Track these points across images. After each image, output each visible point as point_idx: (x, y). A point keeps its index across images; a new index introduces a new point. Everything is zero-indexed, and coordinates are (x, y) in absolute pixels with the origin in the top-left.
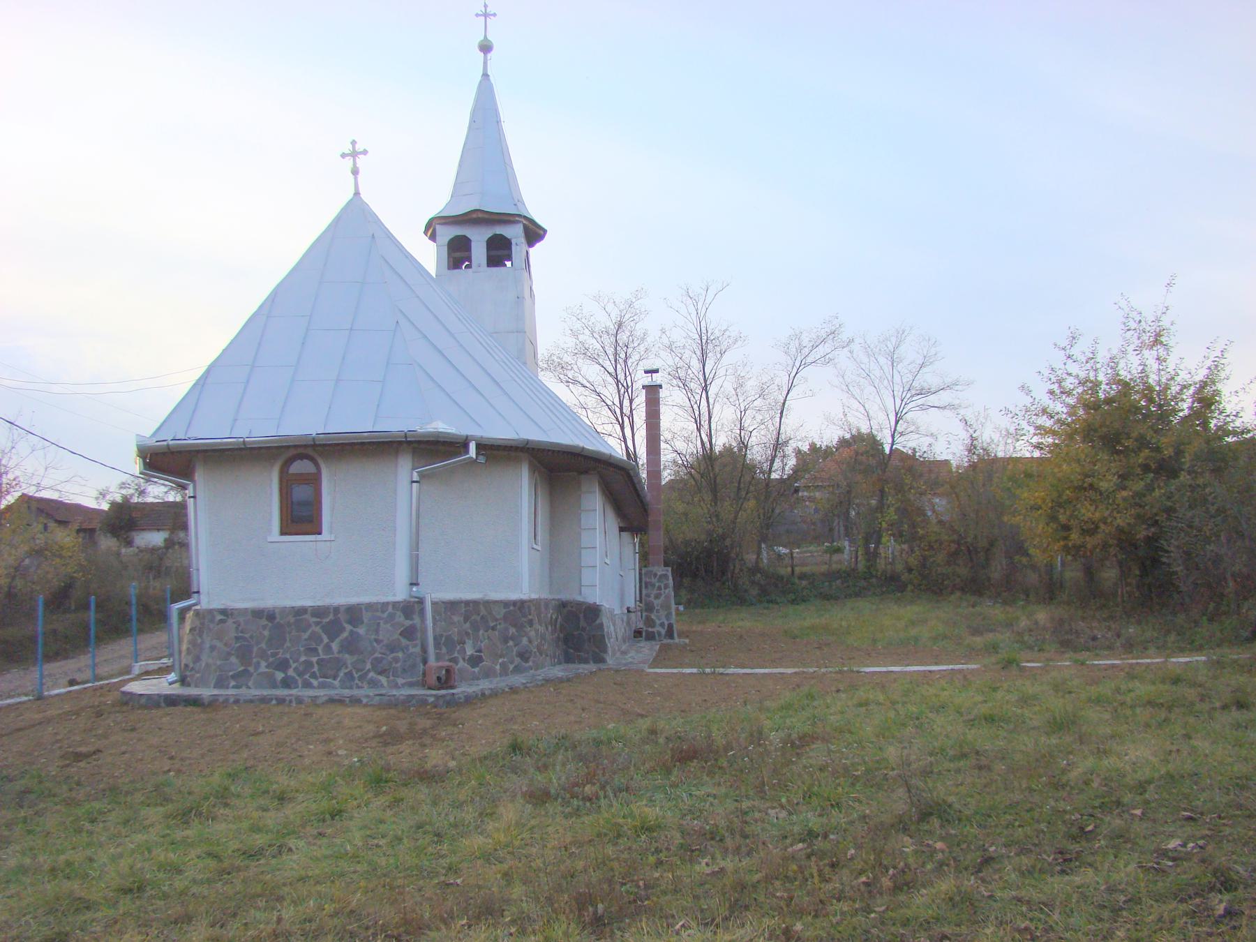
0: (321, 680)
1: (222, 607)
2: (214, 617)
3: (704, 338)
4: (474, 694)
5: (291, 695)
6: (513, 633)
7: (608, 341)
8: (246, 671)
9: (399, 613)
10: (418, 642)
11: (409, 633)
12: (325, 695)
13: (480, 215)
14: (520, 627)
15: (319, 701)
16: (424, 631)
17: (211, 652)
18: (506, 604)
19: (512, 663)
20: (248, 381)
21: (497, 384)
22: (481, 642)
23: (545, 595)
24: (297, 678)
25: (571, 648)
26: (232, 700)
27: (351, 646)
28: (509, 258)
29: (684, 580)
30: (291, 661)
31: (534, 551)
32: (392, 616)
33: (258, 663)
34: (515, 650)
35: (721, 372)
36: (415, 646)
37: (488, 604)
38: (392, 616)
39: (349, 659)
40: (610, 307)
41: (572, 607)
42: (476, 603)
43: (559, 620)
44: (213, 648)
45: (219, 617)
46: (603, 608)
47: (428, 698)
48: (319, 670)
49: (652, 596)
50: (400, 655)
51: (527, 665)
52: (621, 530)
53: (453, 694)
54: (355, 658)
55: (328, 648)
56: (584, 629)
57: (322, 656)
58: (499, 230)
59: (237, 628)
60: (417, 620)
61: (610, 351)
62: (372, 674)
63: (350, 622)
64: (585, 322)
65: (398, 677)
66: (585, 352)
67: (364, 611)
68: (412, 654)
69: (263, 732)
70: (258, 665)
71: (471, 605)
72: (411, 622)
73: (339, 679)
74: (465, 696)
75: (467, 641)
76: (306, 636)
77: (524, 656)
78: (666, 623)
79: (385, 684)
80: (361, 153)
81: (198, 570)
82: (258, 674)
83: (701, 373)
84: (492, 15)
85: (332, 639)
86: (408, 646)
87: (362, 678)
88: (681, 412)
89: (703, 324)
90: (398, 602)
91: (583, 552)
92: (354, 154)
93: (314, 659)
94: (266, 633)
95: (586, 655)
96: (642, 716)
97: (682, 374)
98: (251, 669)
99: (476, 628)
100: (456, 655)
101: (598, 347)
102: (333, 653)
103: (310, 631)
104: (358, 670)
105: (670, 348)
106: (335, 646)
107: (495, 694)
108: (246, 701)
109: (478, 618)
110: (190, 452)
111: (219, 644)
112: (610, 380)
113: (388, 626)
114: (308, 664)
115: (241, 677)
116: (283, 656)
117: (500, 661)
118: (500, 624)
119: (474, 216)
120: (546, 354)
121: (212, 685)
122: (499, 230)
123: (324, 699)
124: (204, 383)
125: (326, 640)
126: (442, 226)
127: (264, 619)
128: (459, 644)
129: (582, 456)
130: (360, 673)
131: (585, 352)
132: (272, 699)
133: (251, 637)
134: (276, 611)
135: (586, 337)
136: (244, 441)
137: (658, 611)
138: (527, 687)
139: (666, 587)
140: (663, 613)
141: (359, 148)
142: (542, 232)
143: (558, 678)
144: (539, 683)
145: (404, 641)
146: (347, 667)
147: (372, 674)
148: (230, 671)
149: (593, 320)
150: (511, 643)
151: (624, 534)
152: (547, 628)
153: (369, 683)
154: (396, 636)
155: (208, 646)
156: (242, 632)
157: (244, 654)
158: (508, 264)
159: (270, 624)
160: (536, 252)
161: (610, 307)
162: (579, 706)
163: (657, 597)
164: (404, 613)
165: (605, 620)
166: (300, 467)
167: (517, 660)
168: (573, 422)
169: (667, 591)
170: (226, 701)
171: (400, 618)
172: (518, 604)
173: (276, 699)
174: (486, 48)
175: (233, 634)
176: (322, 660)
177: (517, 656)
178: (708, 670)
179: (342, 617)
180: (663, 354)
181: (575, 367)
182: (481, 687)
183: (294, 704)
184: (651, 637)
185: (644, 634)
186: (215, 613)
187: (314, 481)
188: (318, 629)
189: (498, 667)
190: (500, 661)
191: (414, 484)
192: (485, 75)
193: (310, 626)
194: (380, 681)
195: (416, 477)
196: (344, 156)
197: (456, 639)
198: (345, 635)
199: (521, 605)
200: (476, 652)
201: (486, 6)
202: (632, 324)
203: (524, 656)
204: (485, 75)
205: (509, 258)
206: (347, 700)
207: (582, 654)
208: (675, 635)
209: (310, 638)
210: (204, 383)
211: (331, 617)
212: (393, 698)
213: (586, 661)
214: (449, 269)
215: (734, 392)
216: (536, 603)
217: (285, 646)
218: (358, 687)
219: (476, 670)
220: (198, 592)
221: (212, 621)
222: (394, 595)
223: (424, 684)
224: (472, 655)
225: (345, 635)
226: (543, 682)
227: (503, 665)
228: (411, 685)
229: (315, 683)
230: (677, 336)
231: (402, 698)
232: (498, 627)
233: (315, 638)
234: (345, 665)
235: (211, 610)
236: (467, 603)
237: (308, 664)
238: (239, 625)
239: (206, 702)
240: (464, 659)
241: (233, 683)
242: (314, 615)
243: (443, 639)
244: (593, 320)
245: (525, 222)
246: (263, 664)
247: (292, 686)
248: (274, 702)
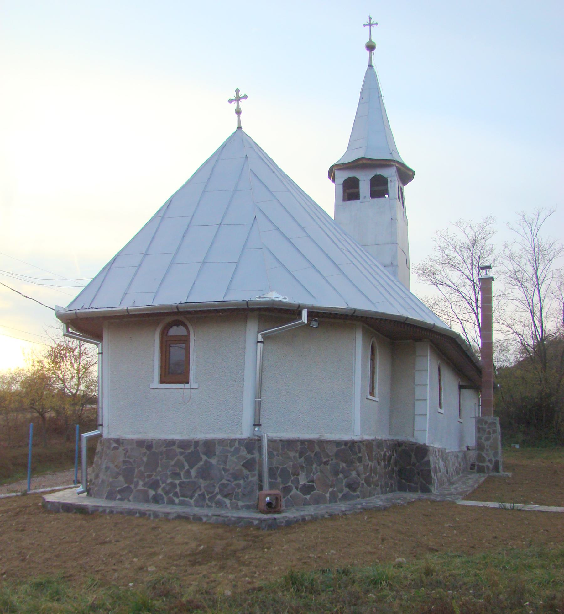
0: (181, 498)
1: (117, 437)
2: (110, 444)
3: (536, 249)
4: (295, 519)
5: (150, 510)
6: (343, 468)
7: (467, 254)
8: (128, 487)
9: (242, 448)
10: (256, 472)
11: (249, 465)
12: (175, 512)
13: (365, 161)
14: (350, 463)
15: (171, 517)
16: (261, 465)
17: (106, 471)
18: (338, 443)
19: (341, 491)
20: (140, 265)
21: (337, 266)
22: (314, 474)
23: (383, 435)
24: (164, 496)
25: (404, 479)
26: (108, 511)
27: (205, 473)
28: (387, 194)
29: (521, 427)
30: (161, 482)
31: (369, 401)
32: (237, 450)
33: (138, 482)
34: (344, 481)
35: (550, 275)
36: (254, 476)
37: (322, 443)
38: (237, 450)
39: (203, 483)
40: (468, 230)
41: (406, 446)
42: (310, 442)
43: (393, 457)
44: (108, 468)
45: (114, 445)
46: (431, 449)
47: (253, 521)
48: (180, 490)
49: (483, 438)
50: (242, 482)
51: (355, 494)
52: (461, 387)
53: (275, 519)
54: (208, 482)
55: (188, 473)
56: (414, 465)
57: (184, 480)
58: (380, 172)
59: (125, 454)
60: (256, 455)
61: (469, 262)
62: (219, 497)
63: (205, 454)
64: (450, 241)
65: (239, 500)
66: (450, 263)
67: (217, 446)
68: (251, 481)
69: (110, 542)
70: (137, 484)
71: (306, 443)
72: (252, 456)
73: (194, 499)
74: (286, 521)
75: (300, 473)
76: (173, 463)
77: (352, 486)
78: (493, 460)
79: (229, 505)
80: (242, 98)
81: (102, 408)
82: (137, 491)
83: (535, 276)
84: (374, 24)
85: (191, 467)
86: (248, 475)
87: (211, 499)
88: (520, 305)
89: (536, 240)
90: (243, 439)
91: (417, 403)
92: (238, 99)
93: (177, 482)
94: (145, 459)
95: (415, 486)
96: (432, 550)
97: (519, 276)
98: (132, 486)
99: (309, 462)
100: (290, 484)
101: (460, 258)
102: (192, 479)
103: (176, 459)
104: (209, 493)
105: (511, 257)
106: (193, 472)
107: (314, 519)
108: (118, 513)
109: (312, 455)
110: (98, 318)
111: (112, 466)
112: (468, 282)
113: (234, 459)
114: (173, 485)
115: (125, 493)
116: (155, 478)
117: (331, 490)
118: (332, 460)
119: (361, 162)
120: (421, 264)
121: (105, 497)
122: (380, 172)
123: (175, 515)
124: (110, 268)
125: (187, 467)
126: (337, 171)
127: (144, 448)
128: (294, 475)
129: (406, 324)
130: (210, 496)
131: (450, 263)
132: (136, 513)
133: (135, 461)
134: (154, 442)
135: (450, 251)
136: (76, 313)
137: (487, 450)
138: (345, 515)
139: (494, 432)
140: (491, 453)
141: (241, 94)
142: (411, 173)
143: (375, 507)
144: (358, 511)
145: (246, 472)
146: (201, 490)
147: (219, 497)
148: (118, 487)
149: (455, 239)
150: (341, 476)
151: (464, 391)
152: (379, 464)
153: (216, 504)
154: (239, 467)
155: (104, 466)
156: (129, 457)
157: (128, 474)
158: (386, 196)
159: (148, 452)
160: (408, 189)
161: (468, 230)
162: (380, 537)
163: (487, 439)
164: (247, 448)
165: (431, 458)
166: (175, 331)
167: (346, 490)
168: (407, 300)
169: (495, 435)
170: (104, 511)
171: (244, 453)
172: (349, 445)
173: (140, 513)
174: (371, 47)
175: (122, 459)
176: (183, 483)
177: (346, 486)
178: (508, 505)
179: (200, 449)
180: (506, 262)
181: (443, 273)
182: (302, 513)
183: (152, 518)
184: (481, 470)
185: (476, 467)
186: (111, 441)
187: (185, 340)
188: (181, 458)
189: (328, 495)
190: (331, 490)
191: (259, 344)
192: (371, 66)
193: (176, 455)
194: (225, 503)
195: (260, 338)
196: (230, 101)
197: (291, 471)
198: (201, 463)
199: (352, 445)
200: (308, 482)
201: (370, 19)
202: (483, 241)
203: (352, 486)
204: (371, 66)
205: (387, 194)
206: (191, 517)
207: (412, 484)
208: (501, 468)
209: (175, 465)
210: (110, 268)
211: (192, 449)
212: (226, 519)
213: (414, 490)
214: (344, 200)
215: (557, 289)
216: (369, 444)
217: (157, 470)
218: (209, 507)
219: (308, 497)
220: (102, 425)
221: (109, 448)
222: (241, 433)
223: (256, 508)
224: (304, 485)
225: (201, 463)
226: (361, 510)
227: (333, 494)
228: (248, 507)
229: (177, 500)
230: (516, 249)
231: (233, 519)
232: (330, 462)
233: (179, 465)
234: (200, 487)
235: (109, 439)
236: (303, 442)
237: (173, 485)
238: (127, 452)
239: (90, 510)
240: (297, 488)
241: (119, 496)
242: (180, 447)
243: (279, 470)
244: (455, 239)
245: (397, 165)
246: (141, 483)
247: (160, 501)
248: (138, 515)
